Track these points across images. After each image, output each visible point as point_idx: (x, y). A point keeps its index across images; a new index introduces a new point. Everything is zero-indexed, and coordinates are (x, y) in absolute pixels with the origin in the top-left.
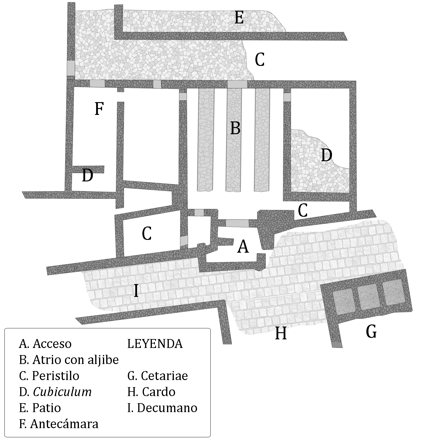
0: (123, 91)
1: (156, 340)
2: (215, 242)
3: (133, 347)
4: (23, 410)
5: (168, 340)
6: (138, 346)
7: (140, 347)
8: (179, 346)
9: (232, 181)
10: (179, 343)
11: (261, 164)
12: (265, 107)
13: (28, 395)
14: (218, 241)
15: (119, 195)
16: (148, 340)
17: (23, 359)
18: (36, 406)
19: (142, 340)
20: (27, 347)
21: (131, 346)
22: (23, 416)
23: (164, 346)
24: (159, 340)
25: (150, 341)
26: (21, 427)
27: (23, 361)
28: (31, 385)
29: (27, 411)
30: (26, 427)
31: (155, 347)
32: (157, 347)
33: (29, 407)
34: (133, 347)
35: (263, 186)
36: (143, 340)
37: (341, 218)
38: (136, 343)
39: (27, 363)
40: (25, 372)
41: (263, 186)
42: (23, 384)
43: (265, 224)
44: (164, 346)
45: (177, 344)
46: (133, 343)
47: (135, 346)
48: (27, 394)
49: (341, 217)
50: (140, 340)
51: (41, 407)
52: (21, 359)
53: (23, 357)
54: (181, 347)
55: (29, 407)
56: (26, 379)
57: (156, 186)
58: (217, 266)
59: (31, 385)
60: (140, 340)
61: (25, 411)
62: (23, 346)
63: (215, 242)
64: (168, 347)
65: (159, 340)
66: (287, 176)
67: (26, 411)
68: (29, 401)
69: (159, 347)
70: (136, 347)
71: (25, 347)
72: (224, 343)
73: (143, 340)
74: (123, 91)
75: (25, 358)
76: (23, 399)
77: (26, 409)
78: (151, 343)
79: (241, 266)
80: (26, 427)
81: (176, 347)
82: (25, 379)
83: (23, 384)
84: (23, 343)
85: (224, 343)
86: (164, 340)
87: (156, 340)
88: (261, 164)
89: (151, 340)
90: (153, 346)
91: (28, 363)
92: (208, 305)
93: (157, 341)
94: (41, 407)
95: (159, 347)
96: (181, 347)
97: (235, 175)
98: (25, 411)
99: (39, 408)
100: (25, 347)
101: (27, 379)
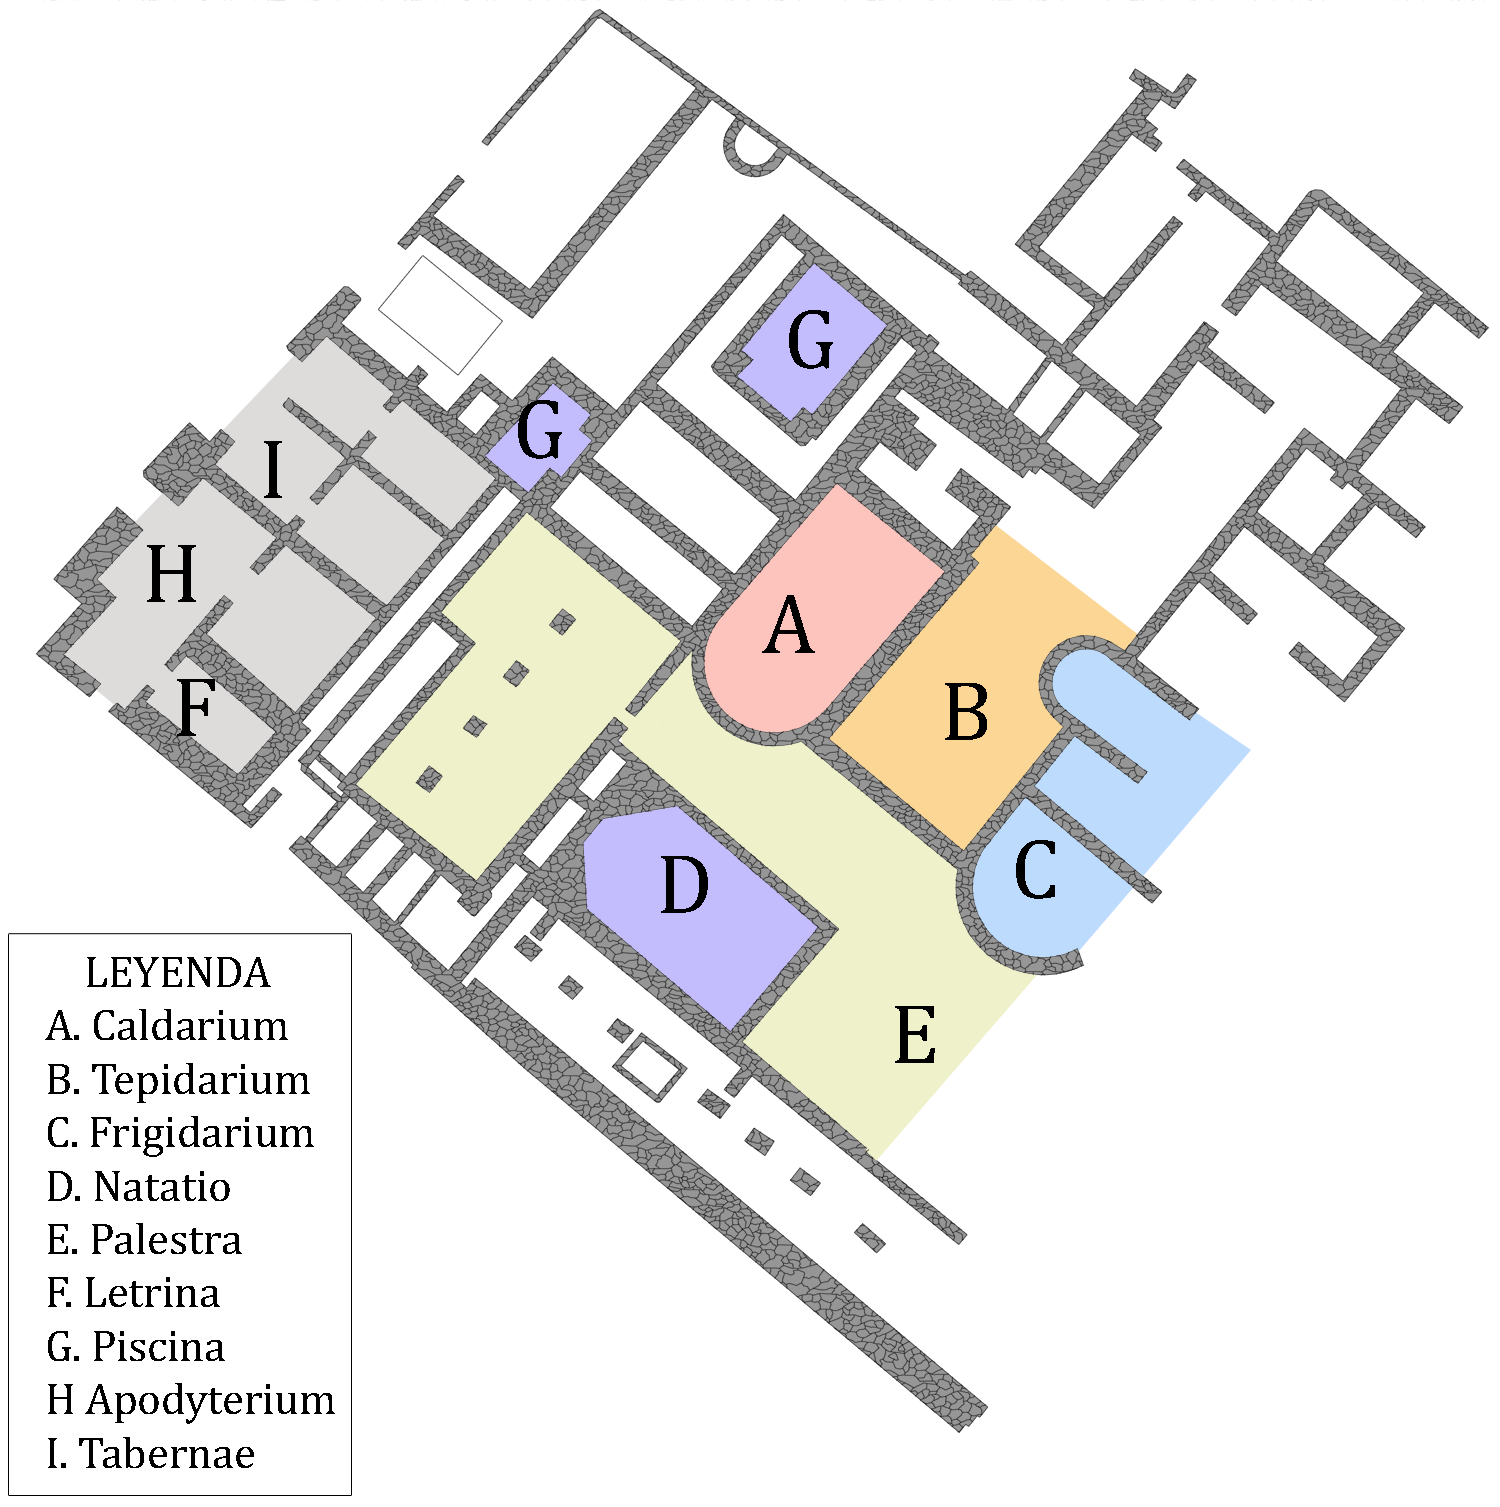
0: (1342, 487)
1: (180, 959)
2: (578, 1087)
3: (105, 984)
4: (59, 1246)
5: (221, 960)
6: (122, 979)
7: (129, 985)
8: (257, 982)
9: (172, 478)
10: (257, 971)
11: (967, 545)
12: (515, 1030)
13: (78, 1199)
14: (574, 1080)
15: (123, 534)
16: (154, 959)
17: (59, 1079)
18: (103, 1233)
19: (133, 960)
20: (72, 1037)
21: (97, 981)
22: (59, 1265)
23: (207, 983)
24: (192, 960)
25: (160, 963)
26: (52, 1304)
27: (59, 1085)
28: (83, 1165)
29: (75, 1252)
30: (69, 1305)
31: (180, 985)
32: (186, 982)
33: (80, 1237)
34: (105, 984)
35: (246, 784)
36: (138, 960)
37: (742, 1222)
38: (115, 971)
39: (71, 1090)
40: (66, 1120)
41: (246, 784)
42: (61, 1159)
43: (241, 788)
44: (207, 983)
45: (251, 975)
46: (103, 971)
47: (110, 982)
48: (73, 1194)
49: (735, 1222)
50: (129, 959)
51: (118, 1236)
52: (52, 1078)
53: (59, 1072)
54: (266, 984)
55: (80, 1237)
56: (70, 1144)
57: (813, 1292)
58: (675, 1169)
59: (83, 1165)
60: (129, 959)
61: (66, 1252)
62: (59, 1035)
63: (578, 1087)
64: (221, 984)
65: (192, 960)
66: (571, 915)
67: (70, 1251)
68: (80, 1216)
69: (190, 985)
70: (115, 984)
71: (67, 1037)
72: (958, 1424)
73: (138, 960)
74: (1342, 487)
75: (66, 1075)
76: (60, 1212)
77: (70, 1243)
78: (166, 971)
79: (675, 1169)
80: (69, 1305)
81: (248, 985)
82: (66, 1144)
83: (61, 1159)
84: (59, 1024)
85: (958, 1424)
86: (208, 959)
87: (180, 959)
88: (967, 545)
89: (166, 960)
90: (173, 979)
91: (77, 1092)
92: (572, 904)
93: (186, 962)
94: (118, 1236)
95: (190, 985)
96: (266, 984)
97: (180, 463)
98: (66, 1252)
99: (114, 1241)
100: (67, 1037)
101: (75, 1145)
